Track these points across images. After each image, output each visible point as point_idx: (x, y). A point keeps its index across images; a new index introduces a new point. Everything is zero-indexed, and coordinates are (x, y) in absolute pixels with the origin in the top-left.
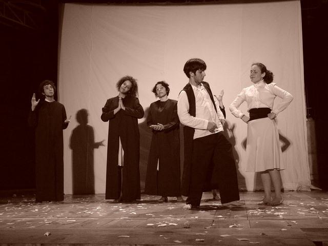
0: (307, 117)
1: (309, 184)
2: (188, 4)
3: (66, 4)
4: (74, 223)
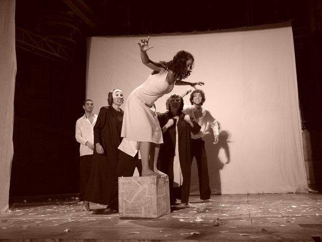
0: (303, 129)
1: (307, 187)
2: (195, 34)
3: (93, 38)
4: (94, 221)
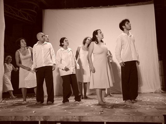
1: (160, 90)
3: (46, 10)
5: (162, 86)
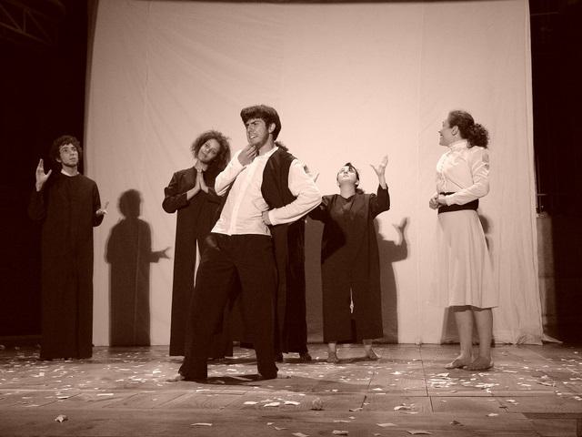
0: (539, 211)
5: (545, 318)
